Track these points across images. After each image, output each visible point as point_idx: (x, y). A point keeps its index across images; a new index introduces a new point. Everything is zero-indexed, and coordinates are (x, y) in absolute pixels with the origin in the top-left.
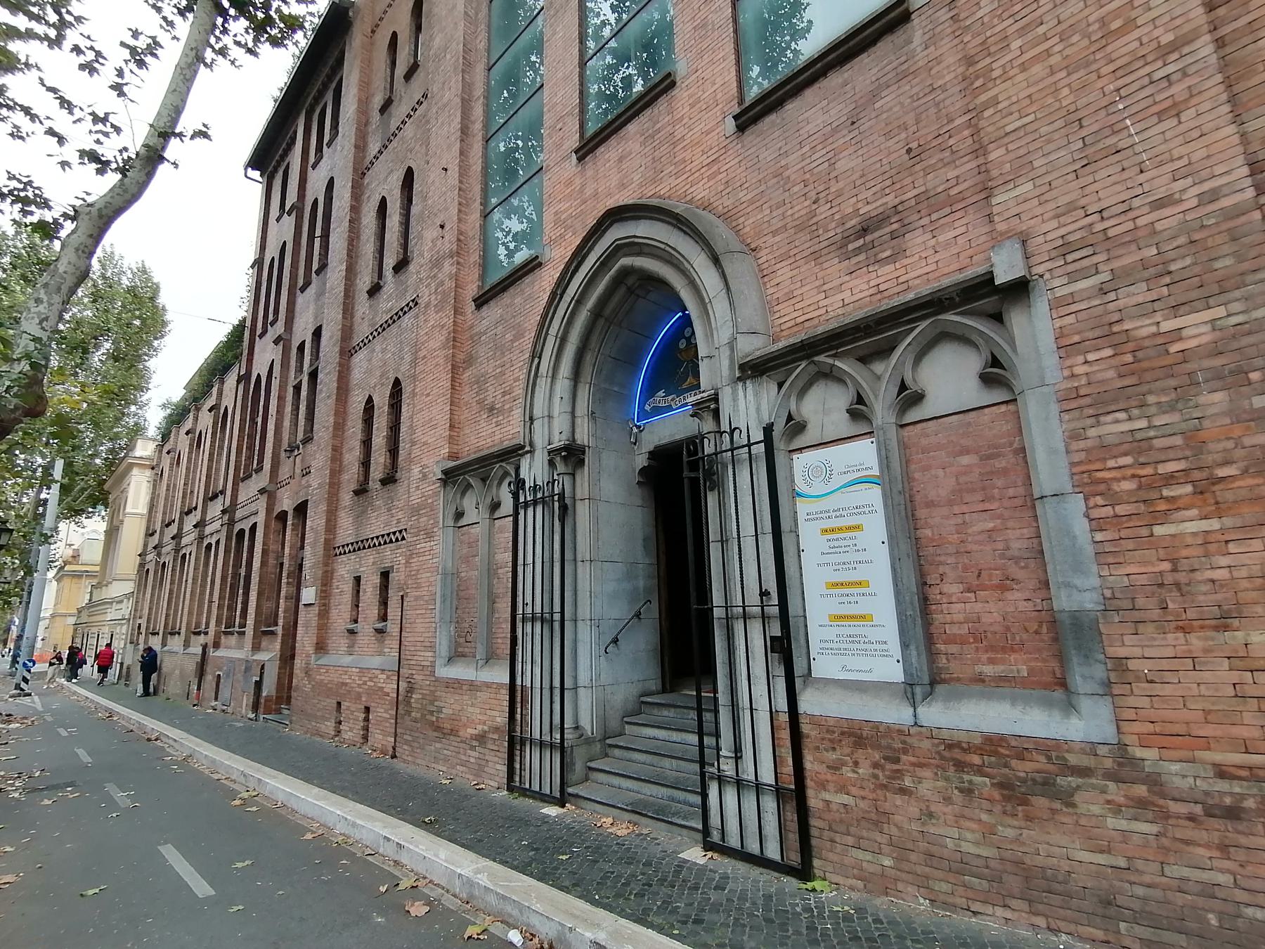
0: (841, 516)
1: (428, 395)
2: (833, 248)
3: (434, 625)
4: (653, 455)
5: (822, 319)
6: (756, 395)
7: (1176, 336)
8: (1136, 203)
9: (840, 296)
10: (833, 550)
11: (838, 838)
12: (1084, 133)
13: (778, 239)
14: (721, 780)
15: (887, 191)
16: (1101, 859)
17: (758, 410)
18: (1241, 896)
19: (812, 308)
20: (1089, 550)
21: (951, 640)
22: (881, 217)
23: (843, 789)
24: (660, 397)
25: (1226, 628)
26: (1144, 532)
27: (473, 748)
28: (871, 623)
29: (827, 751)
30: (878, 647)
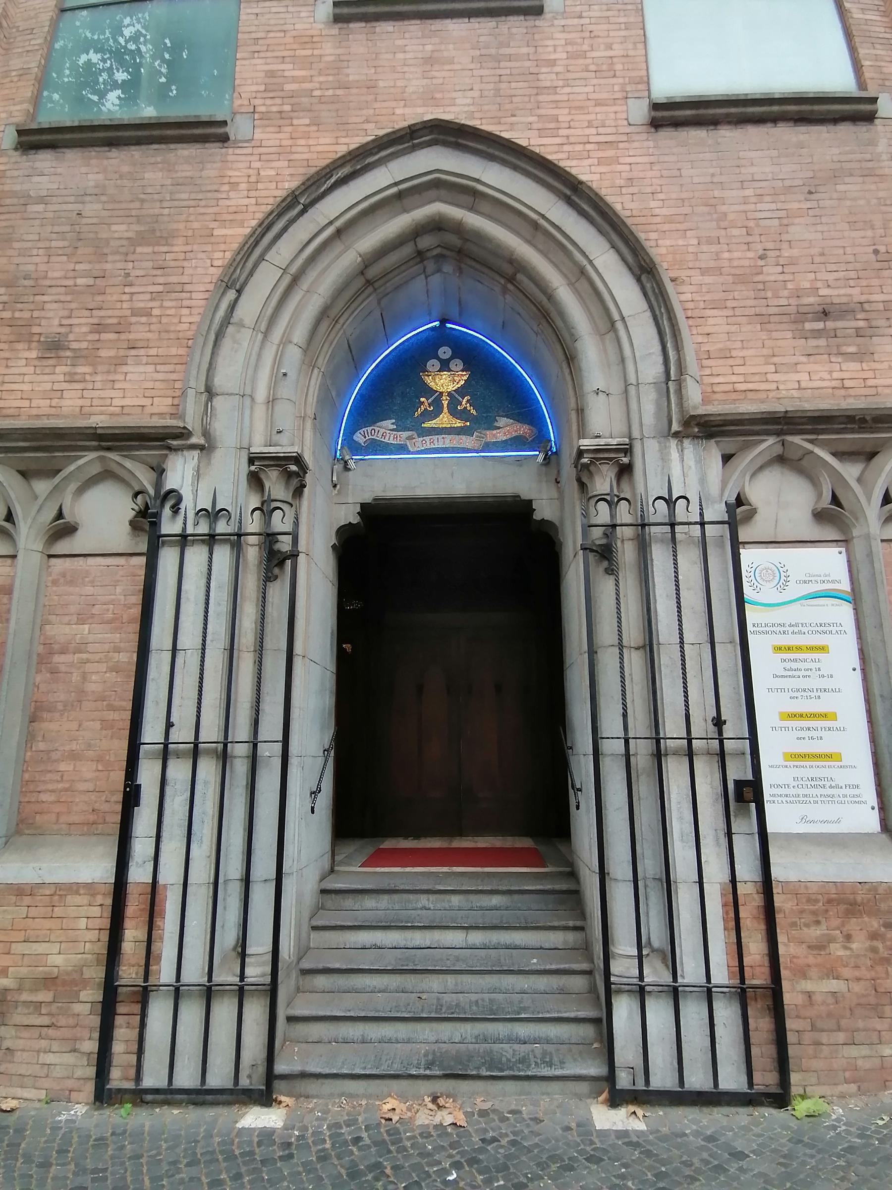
0: (800, 632)
2: (785, 318)
4: (366, 510)
5: (771, 395)
6: (699, 461)
9: (797, 377)
10: (790, 673)
11: (824, 1038)
13: (708, 279)
15: (852, 283)
19: (757, 378)
22: (844, 308)
23: (831, 973)
28: (840, 764)
29: (807, 925)
30: (848, 791)
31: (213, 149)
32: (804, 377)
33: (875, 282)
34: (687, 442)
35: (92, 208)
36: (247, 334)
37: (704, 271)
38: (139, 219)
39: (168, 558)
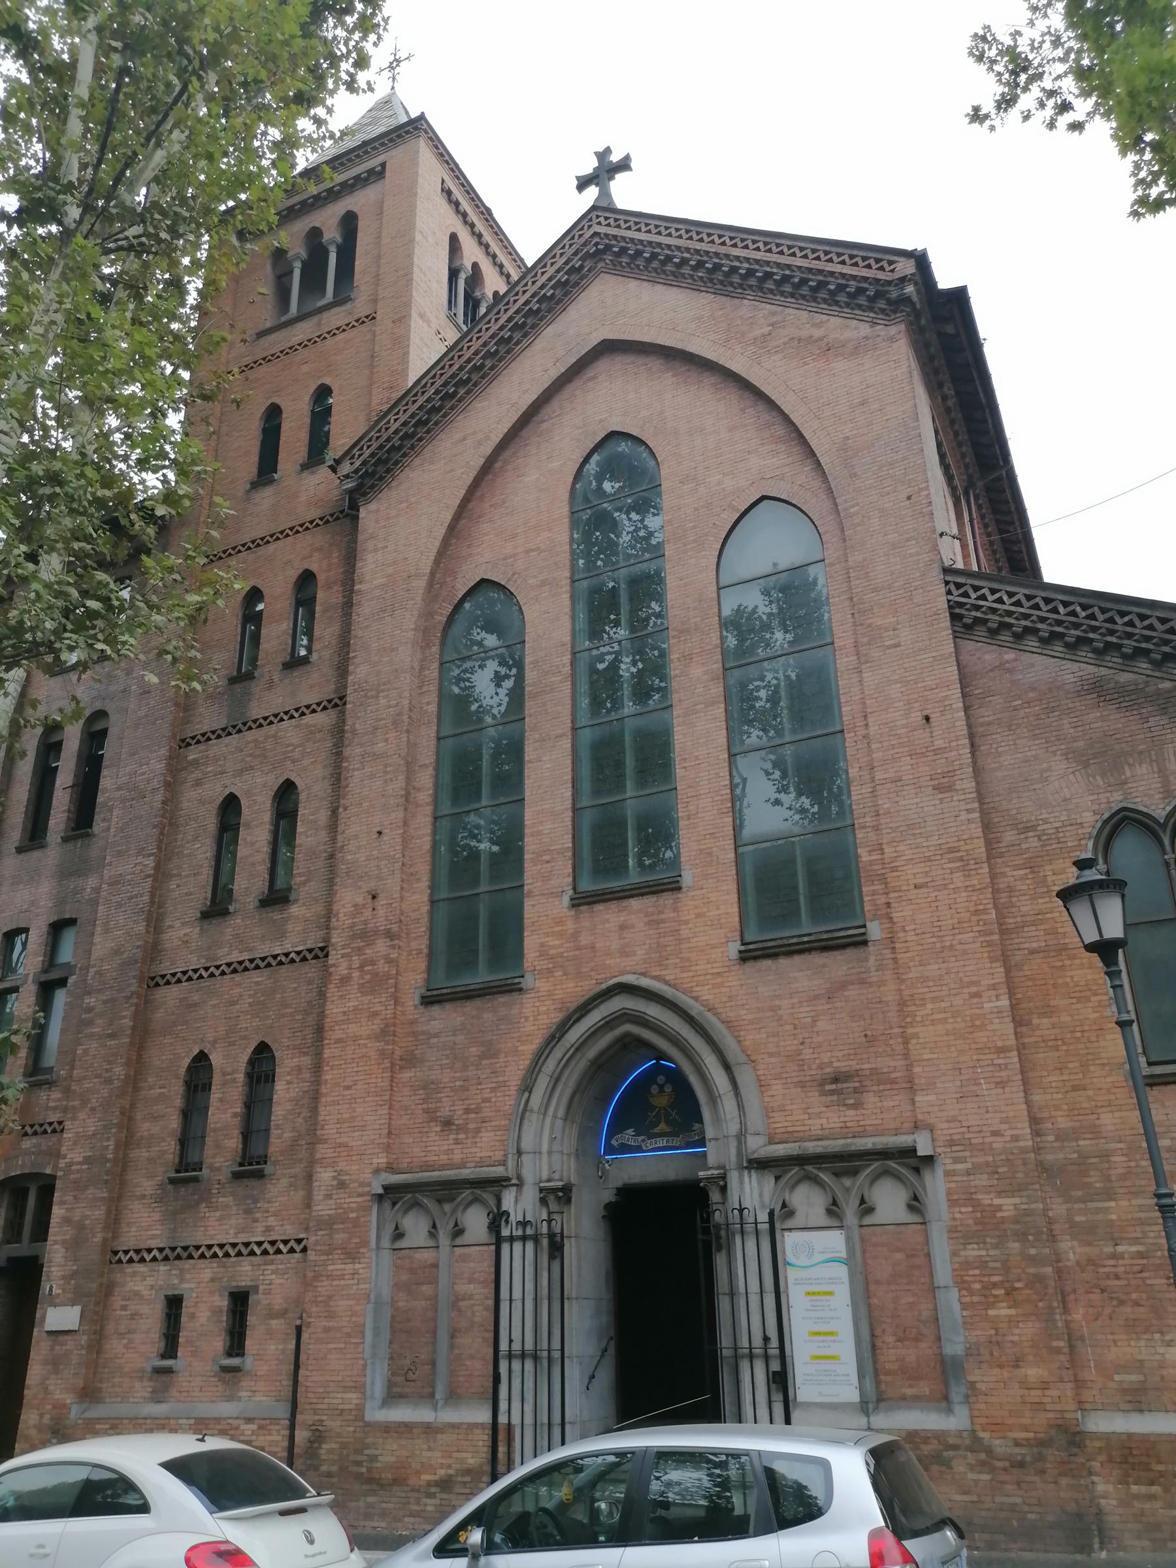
1: (348, 1088)
2: (815, 1084)
3: (361, 1362)
6: (759, 1183)
7: (999, 1208)
8: (985, 1128)
9: (819, 1121)
12: (963, 1077)
13: (773, 1060)
16: (966, 1498)
17: (761, 1195)
18: (1026, 1508)
20: (960, 1321)
21: (888, 1373)
24: (628, 1136)
25: (1018, 1367)
26: (984, 1312)
27: (430, 1495)
31: (515, 995)
32: (824, 1121)
33: (865, 1056)
34: (753, 1171)
35: (460, 1038)
36: (535, 1116)
37: (771, 1055)
39: (505, 1248)
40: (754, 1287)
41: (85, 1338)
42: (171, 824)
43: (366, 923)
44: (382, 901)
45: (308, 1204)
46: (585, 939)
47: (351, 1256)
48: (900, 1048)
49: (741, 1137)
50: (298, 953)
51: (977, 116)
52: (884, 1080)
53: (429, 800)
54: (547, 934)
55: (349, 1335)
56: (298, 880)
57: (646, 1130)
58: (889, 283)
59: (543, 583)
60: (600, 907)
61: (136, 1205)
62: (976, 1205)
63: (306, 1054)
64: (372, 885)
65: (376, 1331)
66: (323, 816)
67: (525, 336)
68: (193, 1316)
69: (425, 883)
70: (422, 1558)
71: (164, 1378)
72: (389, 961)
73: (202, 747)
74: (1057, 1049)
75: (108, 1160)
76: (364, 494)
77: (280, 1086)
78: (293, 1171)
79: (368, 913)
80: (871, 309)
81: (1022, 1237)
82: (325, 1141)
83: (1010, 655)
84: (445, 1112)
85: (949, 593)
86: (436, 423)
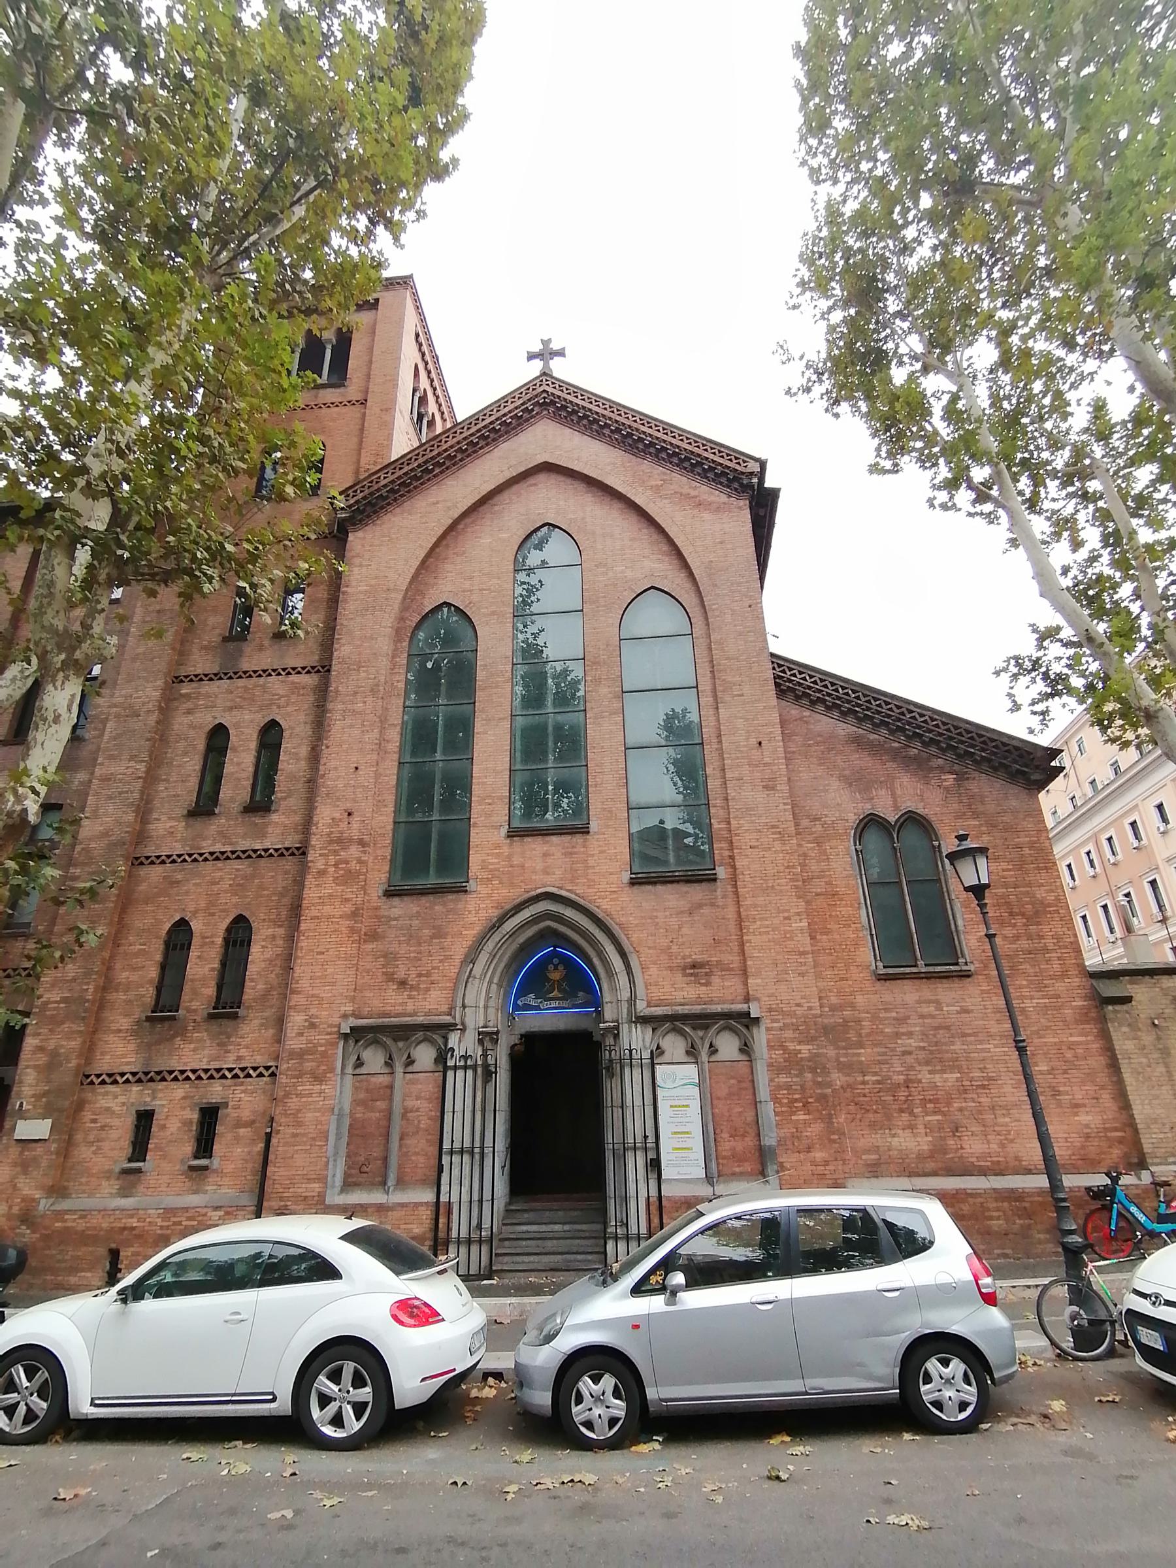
7: (800, 1051)
14: (616, 1239)
24: (531, 999)
31: (462, 896)
35: (415, 922)
36: (477, 981)
37: (650, 948)
38: (434, 927)
39: (450, 1074)
40: (638, 1102)
41: (55, 1145)
42: (161, 740)
43: (341, 833)
44: (356, 818)
45: (279, 1039)
46: (516, 860)
47: (318, 1079)
48: (736, 949)
49: (632, 1000)
50: (276, 850)
51: (788, 392)
52: (725, 968)
53: (397, 750)
54: (488, 855)
55: (314, 1139)
56: (279, 795)
57: (543, 995)
58: (743, 473)
59: (493, 613)
60: (529, 839)
61: (111, 1038)
62: (785, 1049)
63: (280, 926)
64: (348, 805)
65: (338, 1136)
66: (304, 751)
67: (487, 444)
68: (163, 1127)
69: (391, 808)
70: (622, 1296)
71: (132, 1177)
72: (360, 861)
73: (194, 685)
74: (830, 954)
75: (88, 1001)
76: (354, 524)
77: (255, 949)
78: (265, 1014)
79: (344, 825)
80: (729, 487)
81: (813, 1070)
82: (299, 993)
83: (807, 713)
84: (401, 974)
85: (774, 669)
86: (415, 488)
